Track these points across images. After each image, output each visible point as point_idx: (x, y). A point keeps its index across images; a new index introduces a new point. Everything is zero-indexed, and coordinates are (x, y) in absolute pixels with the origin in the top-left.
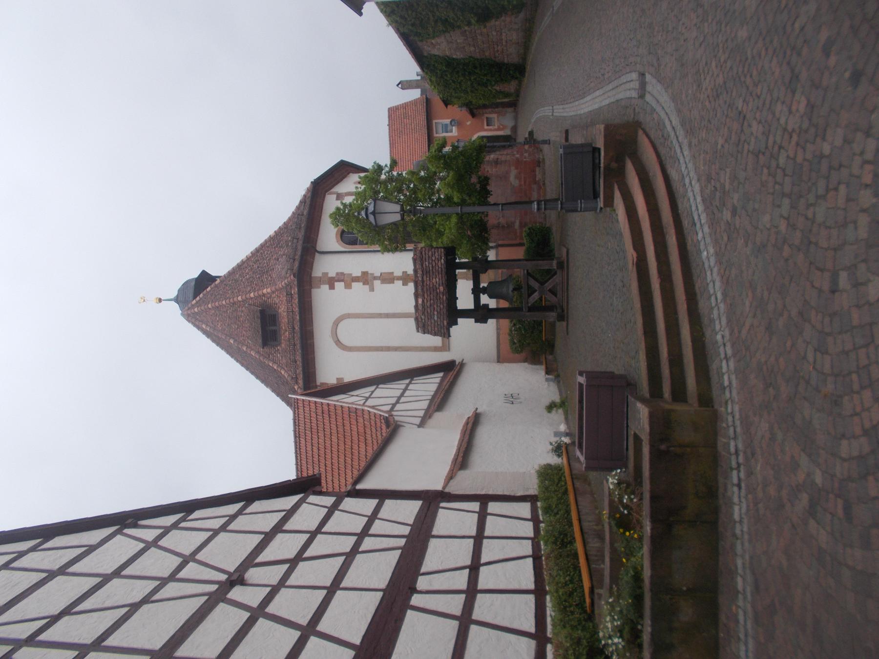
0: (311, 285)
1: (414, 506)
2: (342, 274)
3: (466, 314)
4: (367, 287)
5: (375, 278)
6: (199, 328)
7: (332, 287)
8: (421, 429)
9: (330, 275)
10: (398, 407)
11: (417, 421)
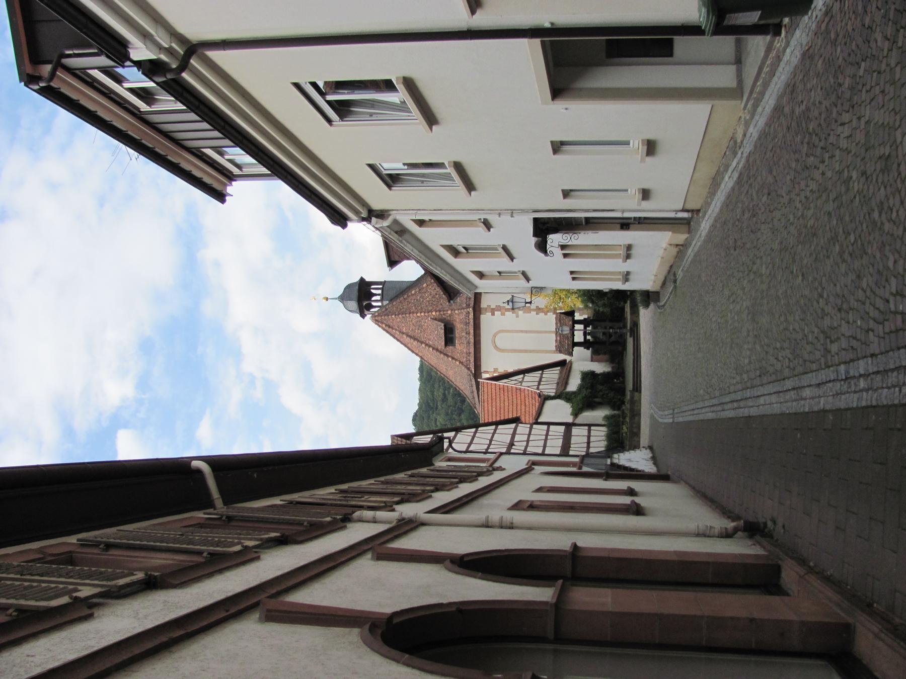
1: (562, 429)
3: (579, 344)
7: (493, 314)
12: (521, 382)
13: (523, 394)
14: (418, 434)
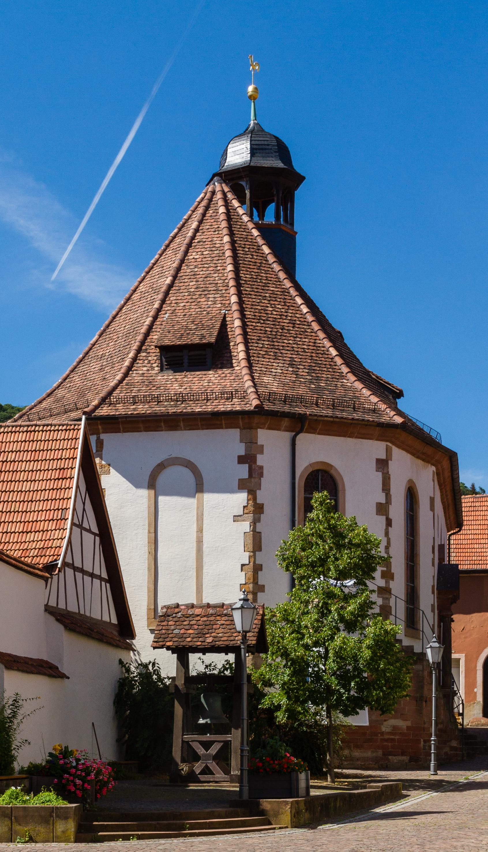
2: (261, 475)
7: (241, 460)
8: (43, 608)
9: (259, 457)
11: (53, 603)
12: (80, 526)
13: (52, 526)
14: (251, 484)
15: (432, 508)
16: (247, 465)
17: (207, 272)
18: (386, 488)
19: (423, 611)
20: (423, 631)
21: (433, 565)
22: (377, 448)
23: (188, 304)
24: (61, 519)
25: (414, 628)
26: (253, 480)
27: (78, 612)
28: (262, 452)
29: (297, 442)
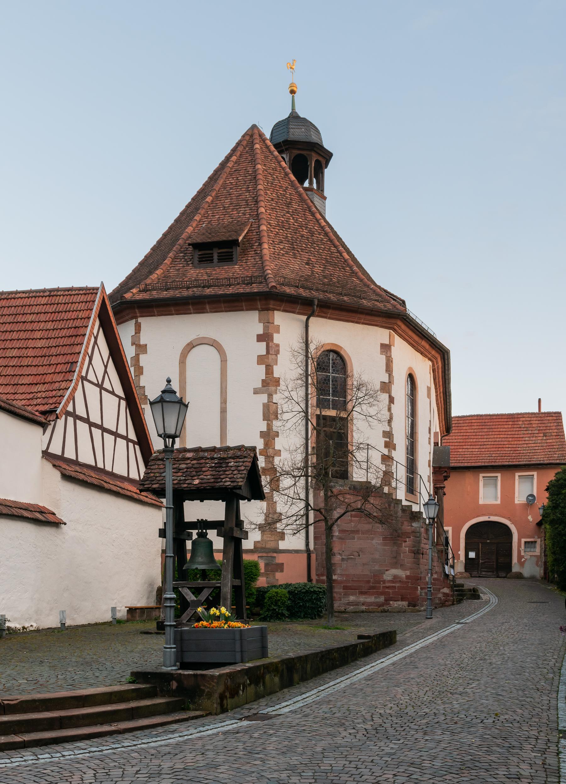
0: (263, 310)
2: (277, 352)
4: (260, 386)
5: (270, 396)
6: (234, 150)
7: (260, 338)
9: (275, 336)
10: (83, 427)
11: (55, 449)
15: (429, 396)
16: (265, 343)
17: (240, 192)
18: (389, 369)
19: (421, 477)
20: (420, 493)
21: (430, 443)
22: (382, 335)
23: (223, 216)
24: (70, 372)
25: (413, 494)
26: (270, 356)
27: (126, 475)
28: (278, 332)
29: (310, 324)
